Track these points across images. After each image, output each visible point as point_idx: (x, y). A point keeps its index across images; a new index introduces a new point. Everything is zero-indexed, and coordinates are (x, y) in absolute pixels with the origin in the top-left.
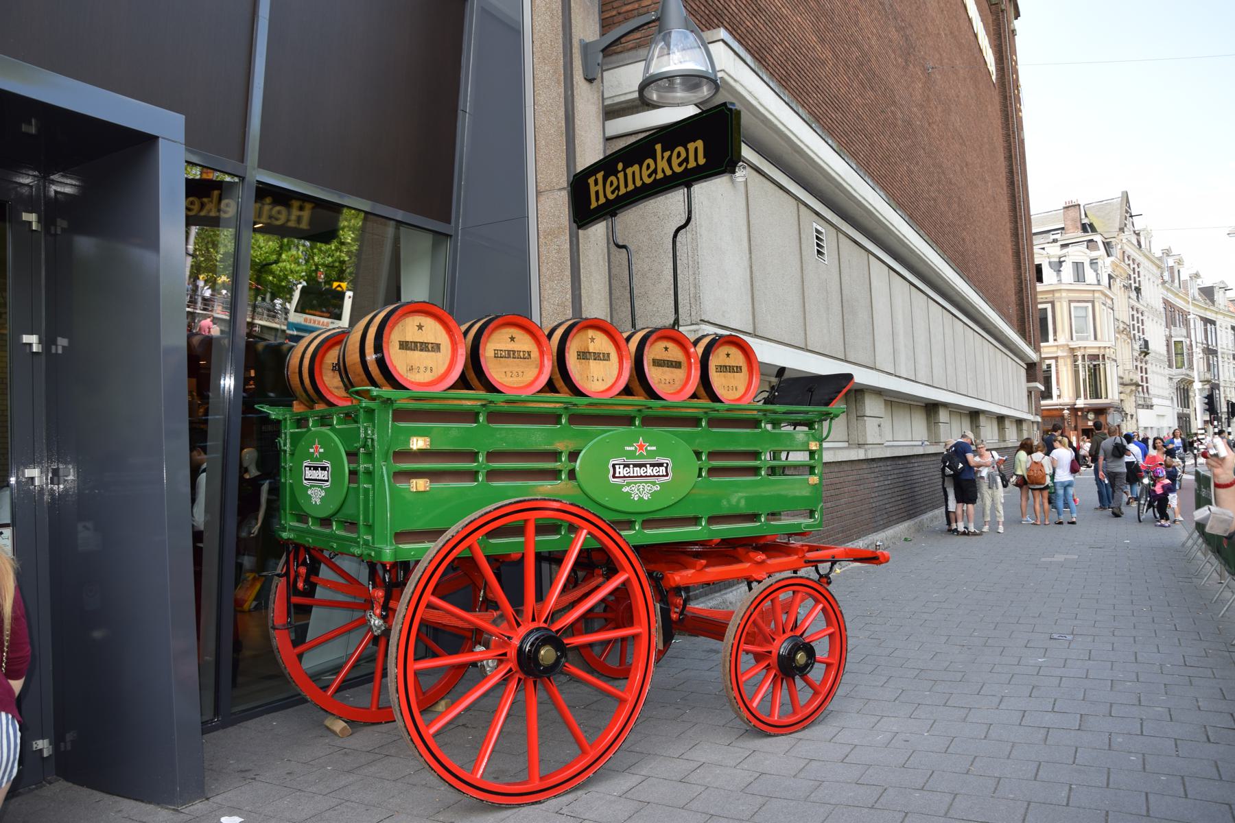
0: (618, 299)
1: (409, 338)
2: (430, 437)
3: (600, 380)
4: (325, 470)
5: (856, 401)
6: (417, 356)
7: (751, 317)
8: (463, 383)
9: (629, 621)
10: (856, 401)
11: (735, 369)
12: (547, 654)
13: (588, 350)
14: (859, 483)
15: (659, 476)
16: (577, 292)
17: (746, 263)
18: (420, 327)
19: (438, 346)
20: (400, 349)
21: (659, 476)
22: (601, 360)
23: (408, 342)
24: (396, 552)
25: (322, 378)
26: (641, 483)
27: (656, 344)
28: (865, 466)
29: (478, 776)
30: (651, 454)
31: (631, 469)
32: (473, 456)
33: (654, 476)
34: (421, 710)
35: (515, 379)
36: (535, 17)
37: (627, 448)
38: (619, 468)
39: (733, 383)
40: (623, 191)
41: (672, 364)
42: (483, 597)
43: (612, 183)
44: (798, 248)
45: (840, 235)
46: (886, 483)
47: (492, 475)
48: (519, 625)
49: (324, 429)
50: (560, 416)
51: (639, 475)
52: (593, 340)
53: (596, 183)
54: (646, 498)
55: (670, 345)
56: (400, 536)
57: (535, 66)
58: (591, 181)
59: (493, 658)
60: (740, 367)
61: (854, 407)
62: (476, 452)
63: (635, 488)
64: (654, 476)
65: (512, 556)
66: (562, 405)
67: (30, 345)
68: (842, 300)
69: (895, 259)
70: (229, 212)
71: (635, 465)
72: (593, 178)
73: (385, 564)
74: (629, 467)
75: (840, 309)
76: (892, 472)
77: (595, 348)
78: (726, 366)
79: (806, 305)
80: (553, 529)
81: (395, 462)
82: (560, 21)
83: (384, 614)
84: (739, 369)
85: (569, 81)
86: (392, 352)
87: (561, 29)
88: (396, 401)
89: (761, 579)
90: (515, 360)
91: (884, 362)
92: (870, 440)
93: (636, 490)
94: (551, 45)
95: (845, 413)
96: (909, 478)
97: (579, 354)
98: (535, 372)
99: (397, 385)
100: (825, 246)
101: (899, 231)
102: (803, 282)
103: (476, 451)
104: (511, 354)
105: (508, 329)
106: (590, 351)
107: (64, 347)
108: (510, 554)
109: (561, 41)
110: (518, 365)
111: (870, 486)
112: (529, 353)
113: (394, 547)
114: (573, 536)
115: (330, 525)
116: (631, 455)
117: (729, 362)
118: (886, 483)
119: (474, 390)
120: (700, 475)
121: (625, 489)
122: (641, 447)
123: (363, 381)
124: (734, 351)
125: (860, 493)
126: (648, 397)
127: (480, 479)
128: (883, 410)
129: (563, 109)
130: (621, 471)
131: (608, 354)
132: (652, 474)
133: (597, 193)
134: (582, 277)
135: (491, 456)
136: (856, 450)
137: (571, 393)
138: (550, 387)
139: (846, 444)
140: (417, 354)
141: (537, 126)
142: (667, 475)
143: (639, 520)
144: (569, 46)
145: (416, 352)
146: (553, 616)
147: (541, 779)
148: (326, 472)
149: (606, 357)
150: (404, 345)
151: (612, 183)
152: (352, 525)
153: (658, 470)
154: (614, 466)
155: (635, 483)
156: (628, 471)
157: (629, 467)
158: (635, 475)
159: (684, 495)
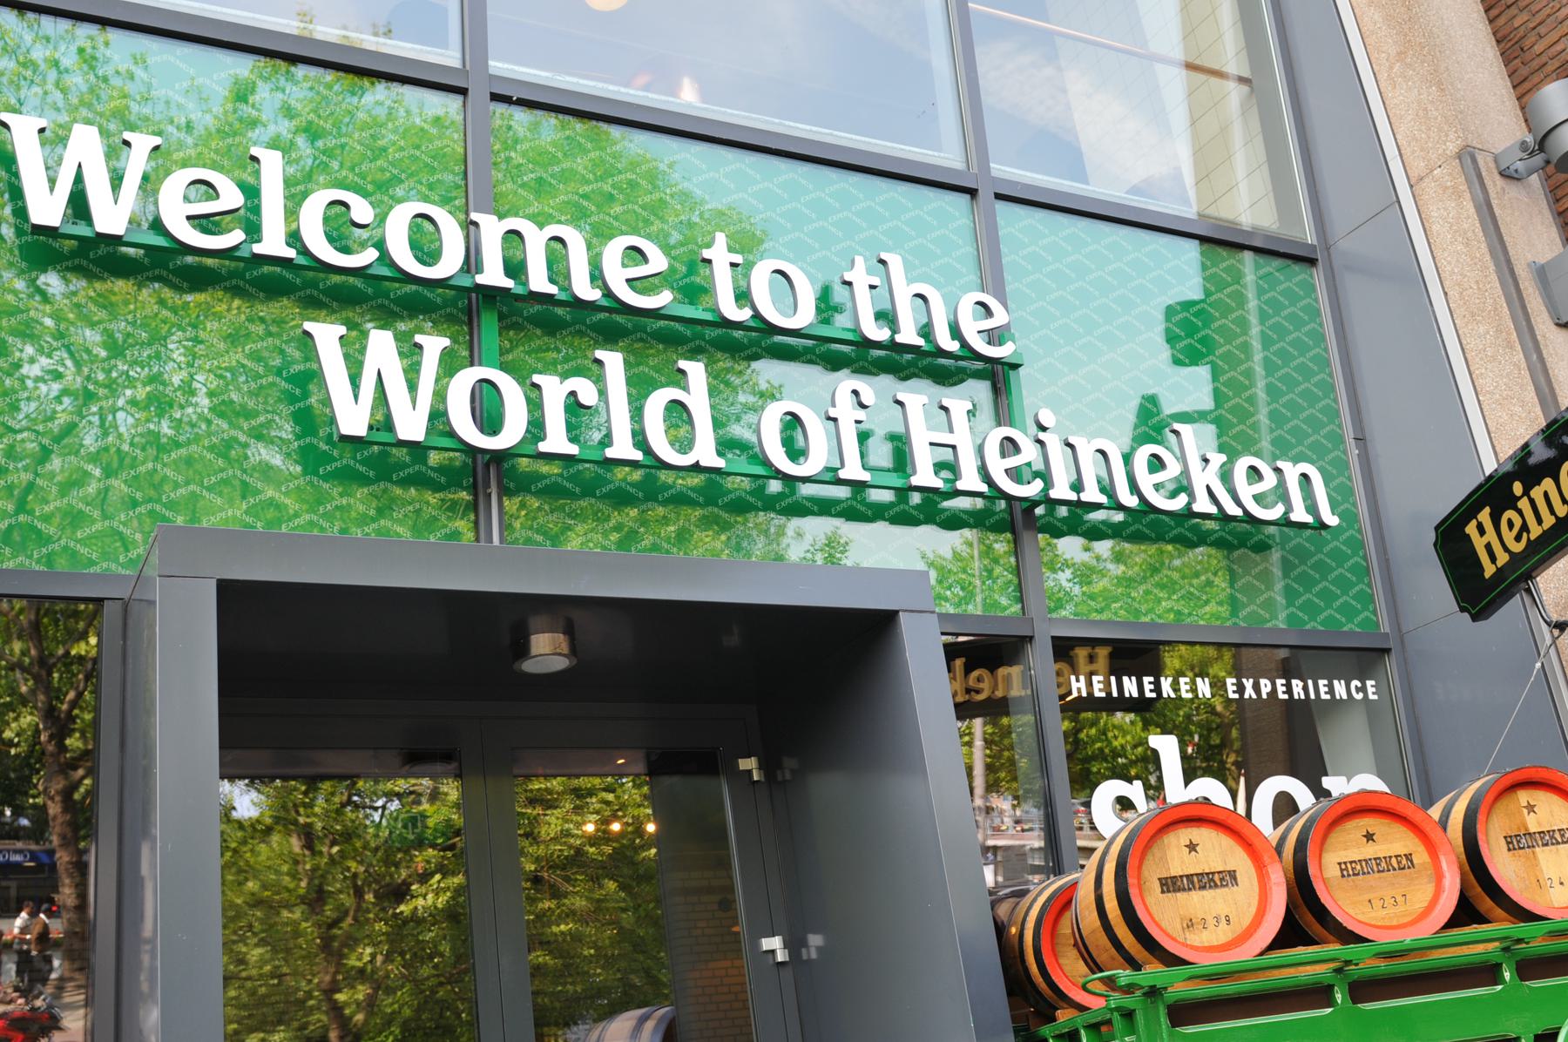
1: (1176, 869)
6: (1197, 902)
8: (1290, 935)
13: (1527, 829)
18: (1192, 847)
19: (1232, 875)
20: (1163, 892)
22: (1558, 843)
23: (1175, 877)
25: (1057, 960)
35: (1391, 911)
36: (1438, 253)
40: (1536, 531)
43: (1511, 525)
52: (1531, 808)
53: (1481, 530)
57: (1460, 332)
58: (1471, 529)
66: (1497, 944)
67: (773, 952)
70: (983, 690)
72: (1474, 523)
77: (1539, 824)
82: (1484, 246)
85: (1527, 337)
86: (1150, 900)
87: (1488, 257)
88: (1166, 988)
90: (1382, 874)
94: (1479, 288)
97: (1509, 840)
99: (1172, 960)
104: (1381, 865)
105: (1357, 821)
106: (1532, 831)
107: (819, 949)
109: (1494, 277)
112: (1408, 857)
119: (1317, 943)
126: (1516, 921)
129: (1531, 388)
133: (1488, 547)
137: (1512, 919)
138: (1465, 913)
141: (1492, 429)
144: (1510, 281)
145: (1193, 893)
150: (1171, 885)
151: (1511, 525)
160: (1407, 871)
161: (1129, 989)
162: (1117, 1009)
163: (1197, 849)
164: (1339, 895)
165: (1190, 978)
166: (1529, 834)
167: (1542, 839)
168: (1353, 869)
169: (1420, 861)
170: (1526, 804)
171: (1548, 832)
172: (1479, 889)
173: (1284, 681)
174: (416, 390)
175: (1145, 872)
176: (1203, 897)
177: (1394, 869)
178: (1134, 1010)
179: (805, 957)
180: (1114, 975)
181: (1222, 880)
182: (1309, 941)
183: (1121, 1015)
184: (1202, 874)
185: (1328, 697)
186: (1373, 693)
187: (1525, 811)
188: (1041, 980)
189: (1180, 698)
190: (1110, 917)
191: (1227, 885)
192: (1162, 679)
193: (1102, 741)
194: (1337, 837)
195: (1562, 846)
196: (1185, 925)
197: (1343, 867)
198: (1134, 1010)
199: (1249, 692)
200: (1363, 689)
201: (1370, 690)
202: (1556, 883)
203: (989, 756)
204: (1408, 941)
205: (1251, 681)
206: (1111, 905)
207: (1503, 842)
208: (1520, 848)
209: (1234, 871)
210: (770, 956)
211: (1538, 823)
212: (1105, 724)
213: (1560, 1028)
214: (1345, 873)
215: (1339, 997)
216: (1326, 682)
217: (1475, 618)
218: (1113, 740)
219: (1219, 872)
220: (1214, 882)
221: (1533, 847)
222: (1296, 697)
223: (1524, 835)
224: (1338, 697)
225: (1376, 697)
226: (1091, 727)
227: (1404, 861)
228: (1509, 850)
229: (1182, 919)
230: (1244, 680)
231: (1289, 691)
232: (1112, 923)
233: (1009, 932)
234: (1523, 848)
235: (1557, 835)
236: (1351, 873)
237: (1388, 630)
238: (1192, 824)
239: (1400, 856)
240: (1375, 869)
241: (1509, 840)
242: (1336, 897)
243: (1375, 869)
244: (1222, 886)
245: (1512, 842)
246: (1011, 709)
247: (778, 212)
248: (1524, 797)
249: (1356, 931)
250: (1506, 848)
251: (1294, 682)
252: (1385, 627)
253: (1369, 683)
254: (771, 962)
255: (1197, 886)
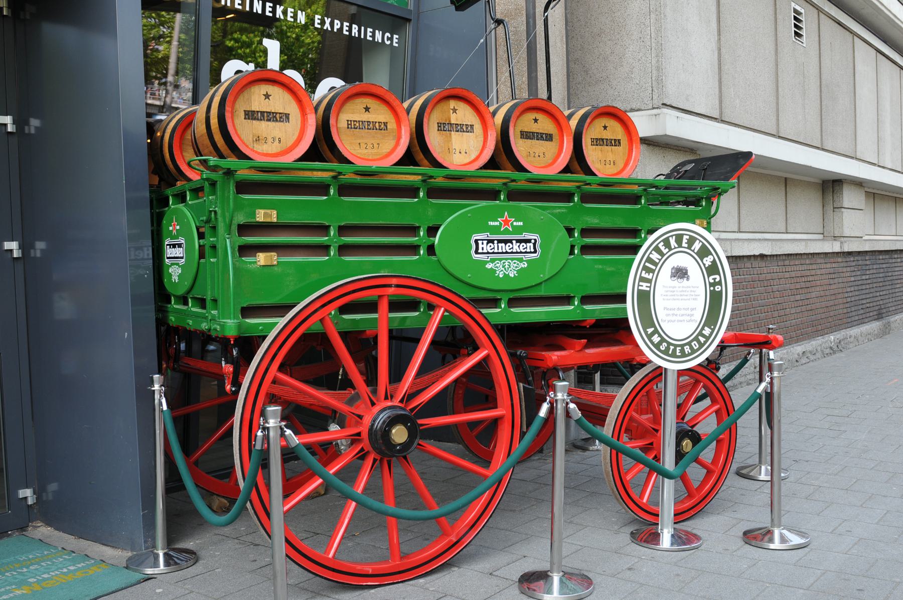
0: (579, 83)
1: (255, 107)
2: (276, 210)
3: (463, 153)
4: (181, 247)
5: (833, 192)
6: (263, 127)
7: (717, 102)
8: (312, 154)
9: (490, 401)
10: (833, 192)
11: (613, 142)
12: (399, 434)
13: (450, 121)
14: (833, 276)
15: (526, 252)
16: (533, 75)
17: (713, 45)
18: (267, 96)
19: (287, 116)
20: (245, 118)
21: (526, 252)
22: (464, 131)
23: (254, 111)
24: (240, 326)
26: (506, 259)
27: (521, 118)
28: (840, 260)
29: (331, 556)
30: (517, 230)
31: (496, 245)
32: (323, 229)
33: (521, 252)
34: (285, 494)
35: (370, 151)
37: (491, 223)
38: (483, 244)
39: (611, 157)
41: (542, 137)
42: (342, 375)
44: (773, 30)
45: (822, 16)
46: (864, 277)
47: (344, 249)
48: (373, 404)
49: (181, 206)
50: (418, 189)
51: (504, 251)
52: (455, 110)
54: (512, 275)
55: (540, 116)
56: (247, 311)
59: (346, 437)
60: (619, 140)
61: (831, 198)
62: (327, 226)
63: (499, 264)
64: (521, 252)
65: (368, 332)
66: (420, 177)
68: (821, 85)
69: (885, 42)
71: (500, 241)
73: (229, 339)
74: (493, 243)
75: (819, 93)
76: (871, 267)
77: (457, 120)
78: (603, 140)
79: (780, 90)
80: (413, 305)
81: (240, 235)
83: (233, 389)
84: (617, 143)
86: (237, 122)
88: (236, 171)
89: (644, 363)
91: (866, 149)
92: (847, 233)
93: (501, 266)
95: (736, 189)
96: (890, 274)
98: (392, 143)
99: (242, 156)
100: (804, 27)
101: (889, 11)
102: (777, 65)
103: (327, 224)
105: (363, 99)
106: (452, 122)
108: (365, 331)
110: (374, 137)
111: (845, 280)
112: (385, 124)
113: (239, 321)
114: (432, 313)
115: (186, 303)
116: (495, 230)
117: (607, 135)
118: (864, 277)
120: (572, 252)
121: (489, 266)
122: (506, 222)
123: (211, 153)
124: (612, 124)
125: (833, 287)
127: (332, 253)
128: (864, 202)
130: (484, 247)
131: (472, 126)
132: (519, 251)
134: (538, 59)
135: (343, 230)
136: (831, 242)
138: (408, 159)
139: (821, 237)
140: (264, 124)
142: (535, 252)
143: (505, 298)
146: (410, 397)
147: (401, 558)
148: (182, 249)
149: (470, 128)
150: (251, 115)
152: (202, 303)
153: (525, 246)
154: (476, 241)
155: (500, 260)
156: (492, 247)
157: (493, 243)
158: (500, 251)
159: (558, 271)
160: (383, 131)
161: (214, 169)
162: (207, 179)
163: (270, 98)
164: (343, 137)
165: (251, 168)
166: (451, 124)
167: (456, 128)
168: (354, 125)
169: (391, 128)
170: (452, 108)
171: (460, 125)
172: (418, 148)
173: (348, 24)
174: (407, 459)
175: (237, 106)
176: (268, 125)
177: (376, 129)
178: (217, 181)
179: (27, 131)
180: (207, 159)
181: (281, 118)
182: (323, 160)
183: (209, 184)
184: (270, 112)
185: (371, 39)
186: (396, 43)
187: (452, 111)
188: (170, 163)
189: (286, 20)
190: (212, 128)
191: (283, 121)
192: (278, 6)
193: (252, 57)
194: (350, 106)
195: (465, 133)
196: (255, 139)
197: (349, 123)
198: (217, 181)
199: (327, 26)
200: (391, 39)
201: (395, 40)
202: (458, 151)
203: (181, 53)
204: (374, 167)
205: (330, 19)
206: (214, 121)
207: (436, 126)
208: (444, 130)
209: (289, 114)
210: (3, 128)
211: (456, 119)
212: (256, 48)
213: (441, 225)
214: (350, 126)
215: (332, 191)
216: (371, 30)
217: (457, 9)
218: (258, 58)
219: (280, 113)
220: (276, 118)
221: (451, 131)
222: (353, 35)
223: (448, 124)
224: (376, 40)
225: (397, 45)
226: (247, 48)
227: (383, 126)
228: (438, 130)
229: (253, 136)
230: (326, 18)
231: (350, 30)
232: (213, 132)
233: (157, 133)
234: (446, 131)
235: (464, 128)
236: (353, 127)
237: (412, 8)
238: (267, 83)
239: (381, 123)
240: (366, 127)
241: (439, 125)
242: (342, 138)
243: (366, 127)
244: (280, 121)
245: (440, 127)
246: (181, 9)
247: (498, 222)
248: (453, 104)
249: (348, 158)
250: (437, 129)
251: (354, 26)
252: (411, 6)
253: (395, 36)
254: (4, 131)
255: (266, 119)
